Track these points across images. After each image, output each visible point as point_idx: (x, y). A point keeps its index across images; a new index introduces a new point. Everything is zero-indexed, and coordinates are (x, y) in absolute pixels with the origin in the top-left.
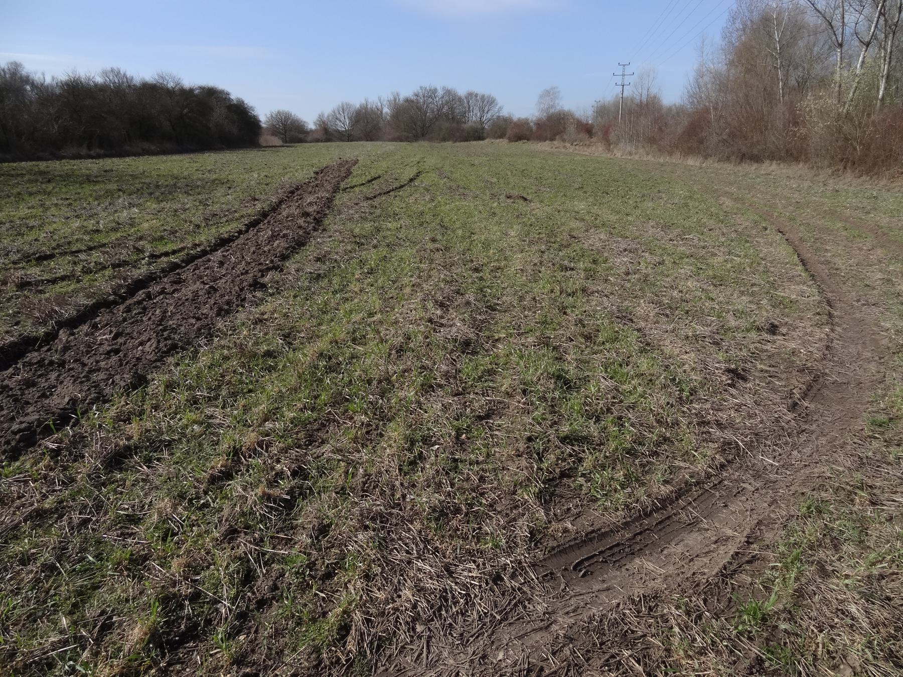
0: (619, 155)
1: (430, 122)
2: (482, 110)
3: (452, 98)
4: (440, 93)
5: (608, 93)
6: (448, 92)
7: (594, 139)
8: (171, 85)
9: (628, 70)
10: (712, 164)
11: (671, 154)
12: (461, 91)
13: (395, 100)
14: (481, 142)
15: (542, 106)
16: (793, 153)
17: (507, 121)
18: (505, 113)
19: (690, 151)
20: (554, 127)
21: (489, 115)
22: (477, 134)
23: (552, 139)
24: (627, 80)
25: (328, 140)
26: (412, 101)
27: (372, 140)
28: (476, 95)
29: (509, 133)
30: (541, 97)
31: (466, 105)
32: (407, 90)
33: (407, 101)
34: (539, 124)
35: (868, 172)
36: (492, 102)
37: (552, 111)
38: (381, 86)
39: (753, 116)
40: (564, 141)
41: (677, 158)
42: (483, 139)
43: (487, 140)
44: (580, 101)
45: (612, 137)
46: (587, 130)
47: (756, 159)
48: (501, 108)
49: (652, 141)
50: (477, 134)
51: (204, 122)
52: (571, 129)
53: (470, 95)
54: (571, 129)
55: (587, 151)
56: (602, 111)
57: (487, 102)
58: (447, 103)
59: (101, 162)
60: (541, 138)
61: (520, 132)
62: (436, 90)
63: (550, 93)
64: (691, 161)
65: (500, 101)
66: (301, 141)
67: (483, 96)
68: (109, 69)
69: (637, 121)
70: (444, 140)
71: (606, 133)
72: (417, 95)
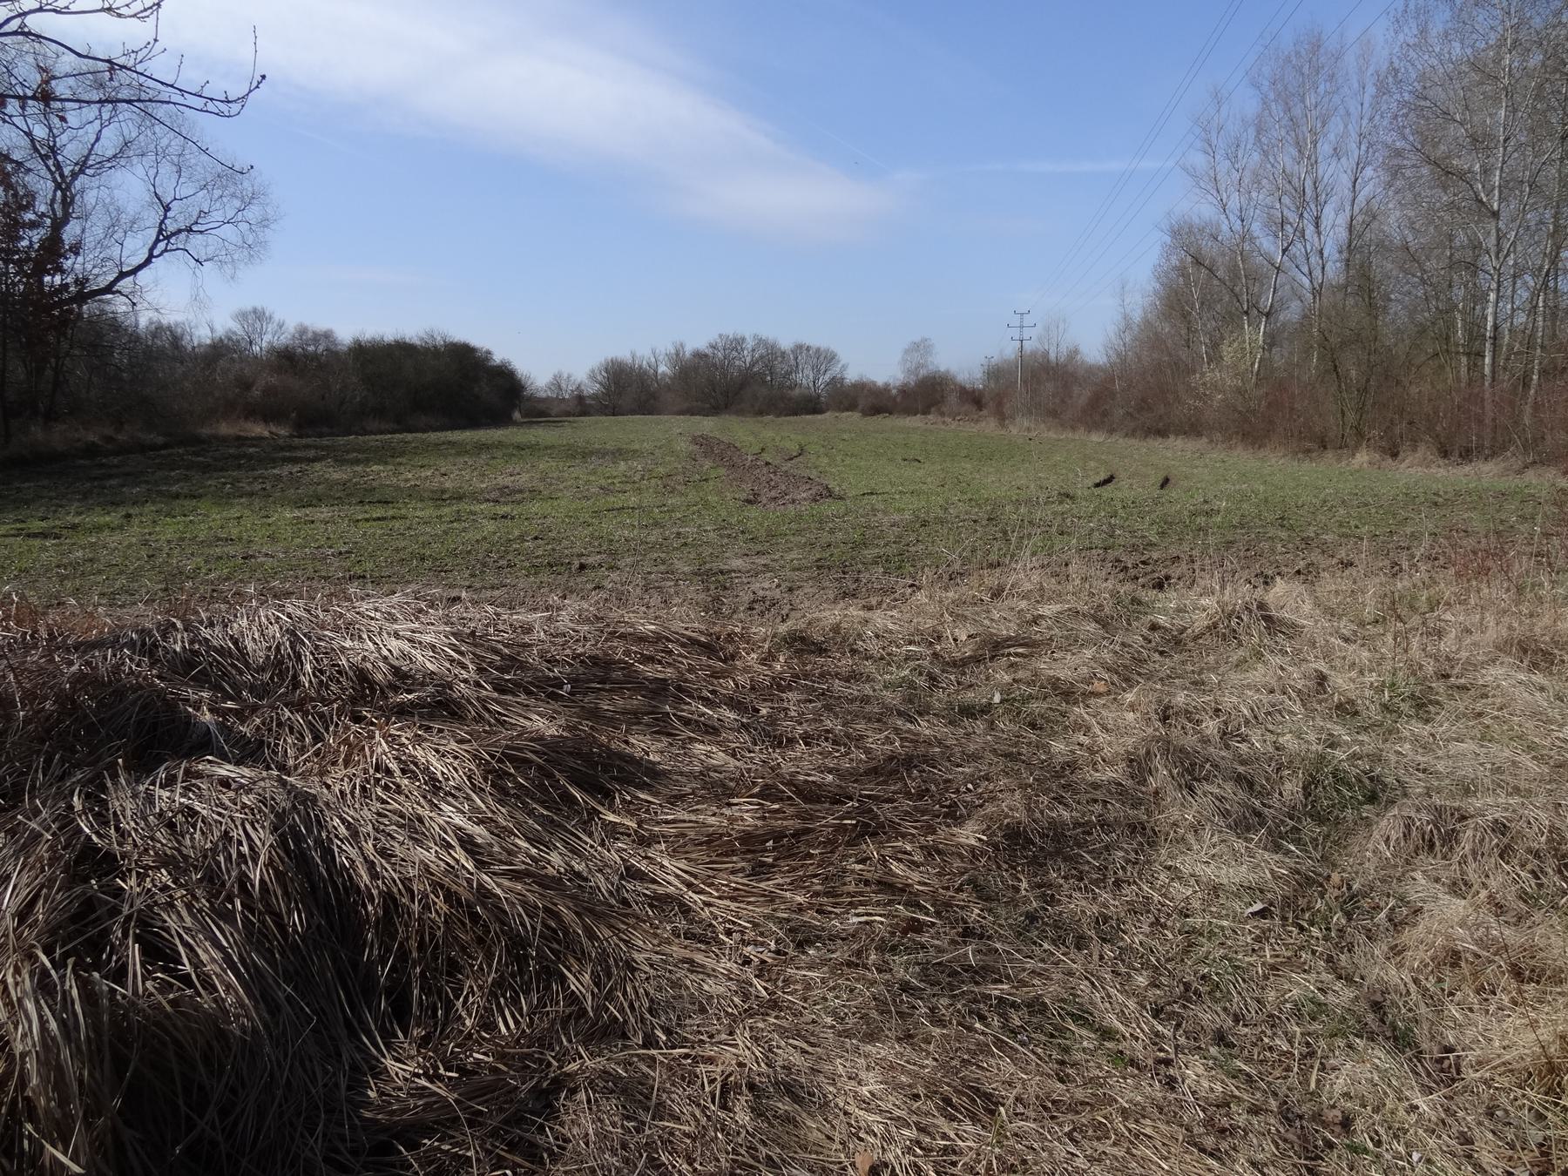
0: (1015, 432)
1: (733, 389)
2: (816, 369)
3: (771, 355)
4: (750, 344)
5: (1002, 348)
6: (761, 342)
7: (985, 412)
8: (439, 341)
9: (1028, 320)
10: (1120, 442)
11: (1073, 428)
12: (786, 343)
13: (677, 354)
14: (819, 417)
15: (908, 365)
16: (1193, 428)
17: (861, 388)
18: (851, 376)
19: (1093, 426)
20: (927, 395)
21: (827, 377)
22: (810, 405)
23: (925, 412)
24: (1027, 333)
25: (584, 413)
26: (706, 356)
27: (650, 413)
28: (808, 349)
29: (862, 403)
30: (907, 352)
31: (793, 362)
32: (698, 338)
33: (699, 355)
34: (904, 391)
35: (1253, 444)
36: (831, 358)
37: (923, 372)
38: (657, 335)
39: (1314, 377)
40: (942, 414)
41: (1080, 434)
42: (821, 412)
43: (828, 414)
44: (965, 356)
45: (1007, 409)
46: (974, 399)
47: (1162, 433)
48: (844, 367)
49: (1054, 414)
50: (810, 405)
51: (453, 391)
52: (953, 399)
53: (799, 348)
54: (953, 399)
55: (974, 429)
56: (995, 373)
57: (824, 358)
58: (761, 357)
59: (397, 436)
60: (910, 411)
61: (875, 402)
62: (743, 339)
63: (921, 347)
64: (1096, 437)
65: (844, 356)
66: (500, 418)
67: (818, 350)
68: (249, 308)
69: (1041, 389)
70: (761, 413)
71: (1000, 404)
72: (714, 347)
